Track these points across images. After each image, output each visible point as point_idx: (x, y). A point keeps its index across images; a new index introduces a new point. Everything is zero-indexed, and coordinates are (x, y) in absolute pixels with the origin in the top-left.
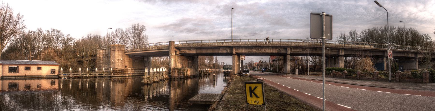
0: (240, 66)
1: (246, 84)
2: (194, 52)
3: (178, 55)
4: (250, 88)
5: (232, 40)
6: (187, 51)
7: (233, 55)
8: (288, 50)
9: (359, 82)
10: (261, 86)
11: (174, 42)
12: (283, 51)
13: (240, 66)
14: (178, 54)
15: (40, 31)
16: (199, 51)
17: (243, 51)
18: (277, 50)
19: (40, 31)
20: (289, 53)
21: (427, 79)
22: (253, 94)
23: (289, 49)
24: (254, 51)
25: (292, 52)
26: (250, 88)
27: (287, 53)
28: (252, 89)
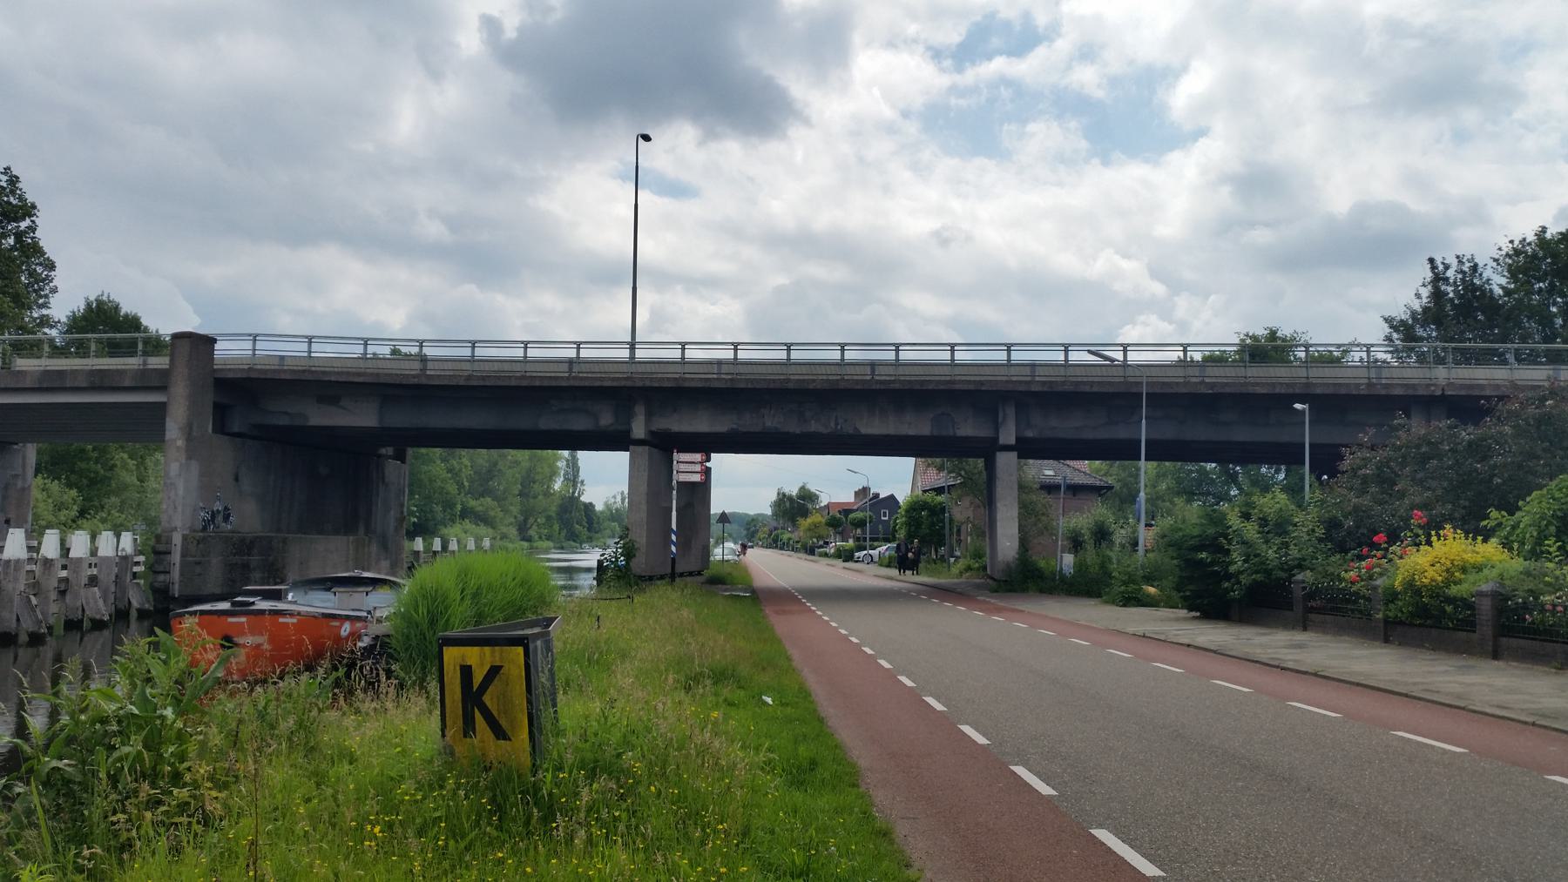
0: (674, 526)
1: (444, 648)
2: (362, 417)
3: (239, 435)
4: (466, 672)
5: (632, 346)
6: (321, 417)
7: (631, 447)
8: (1000, 420)
9: (1283, 638)
10: (1202, 646)
11: (215, 341)
12: (968, 428)
13: (674, 526)
14: (236, 429)
15: (131, 312)
16: (401, 418)
17: (700, 423)
18: (932, 416)
19: (131, 312)
20: (1012, 441)
21: (1486, 629)
22: (477, 714)
23: (1011, 412)
24: (772, 421)
25: (1030, 434)
26: (466, 672)
27: (996, 439)
28: (478, 678)
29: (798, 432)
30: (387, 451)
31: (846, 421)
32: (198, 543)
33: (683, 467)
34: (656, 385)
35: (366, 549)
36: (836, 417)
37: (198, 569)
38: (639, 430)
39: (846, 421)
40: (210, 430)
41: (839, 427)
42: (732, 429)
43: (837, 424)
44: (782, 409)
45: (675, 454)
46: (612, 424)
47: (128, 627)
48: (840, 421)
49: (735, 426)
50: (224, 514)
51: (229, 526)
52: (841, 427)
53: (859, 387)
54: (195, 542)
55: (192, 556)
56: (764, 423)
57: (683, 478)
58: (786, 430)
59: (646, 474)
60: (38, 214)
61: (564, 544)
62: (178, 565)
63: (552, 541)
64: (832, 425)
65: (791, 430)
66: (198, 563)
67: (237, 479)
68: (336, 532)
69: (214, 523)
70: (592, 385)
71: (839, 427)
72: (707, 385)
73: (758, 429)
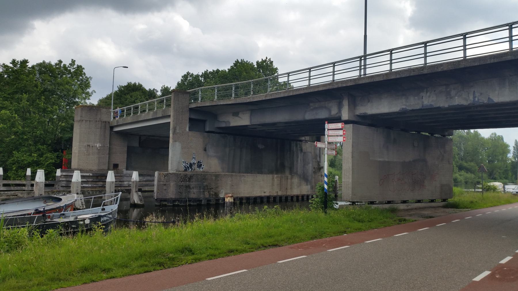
3: (208, 132)
29: (446, 106)
30: (305, 138)
31: (481, 94)
32: (165, 177)
33: (331, 133)
34: (344, 85)
35: (289, 181)
36: (474, 91)
37: (165, 187)
38: (345, 116)
39: (481, 94)
40: (187, 129)
41: (476, 99)
42: (403, 109)
43: (474, 97)
44: (435, 91)
45: (326, 124)
46: (337, 113)
47: (134, 211)
48: (477, 94)
49: (404, 107)
50: (198, 165)
51: (201, 170)
52: (478, 99)
53: (476, 64)
54: (164, 176)
55: (162, 182)
56: (423, 102)
57: (331, 139)
58: (438, 106)
59: (351, 140)
60: (278, 71)
61: (514, 181)
62: (156, 185)
63: (508, 180)
64: (471, 98)
65: (441, 106)
66: (165, 185)
67: (205, 150)
68: (271, 172)
69: (191, 168)
70: (314, 91)
71: (476, 99)
72: (372, 81)
73: (418, 107)
